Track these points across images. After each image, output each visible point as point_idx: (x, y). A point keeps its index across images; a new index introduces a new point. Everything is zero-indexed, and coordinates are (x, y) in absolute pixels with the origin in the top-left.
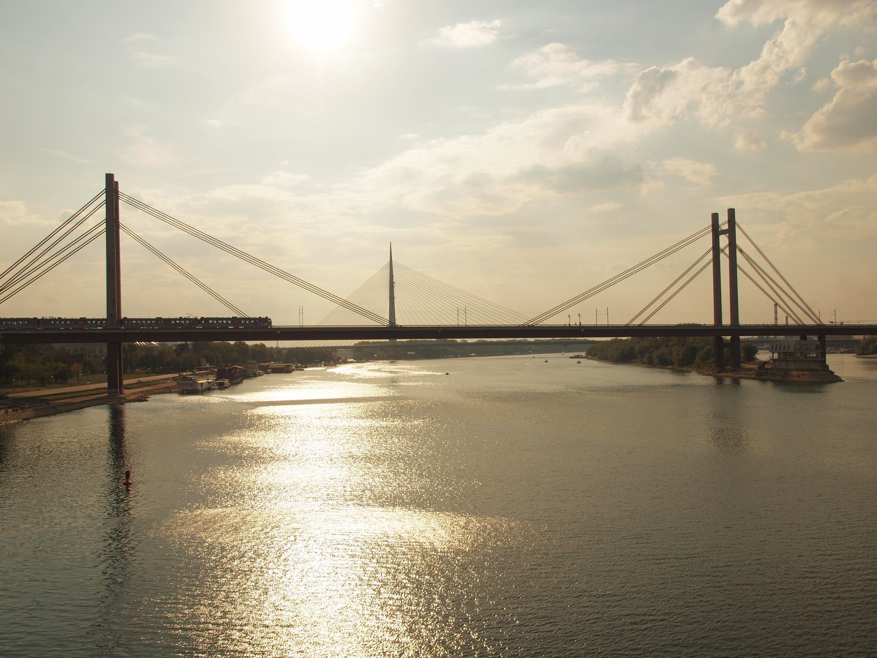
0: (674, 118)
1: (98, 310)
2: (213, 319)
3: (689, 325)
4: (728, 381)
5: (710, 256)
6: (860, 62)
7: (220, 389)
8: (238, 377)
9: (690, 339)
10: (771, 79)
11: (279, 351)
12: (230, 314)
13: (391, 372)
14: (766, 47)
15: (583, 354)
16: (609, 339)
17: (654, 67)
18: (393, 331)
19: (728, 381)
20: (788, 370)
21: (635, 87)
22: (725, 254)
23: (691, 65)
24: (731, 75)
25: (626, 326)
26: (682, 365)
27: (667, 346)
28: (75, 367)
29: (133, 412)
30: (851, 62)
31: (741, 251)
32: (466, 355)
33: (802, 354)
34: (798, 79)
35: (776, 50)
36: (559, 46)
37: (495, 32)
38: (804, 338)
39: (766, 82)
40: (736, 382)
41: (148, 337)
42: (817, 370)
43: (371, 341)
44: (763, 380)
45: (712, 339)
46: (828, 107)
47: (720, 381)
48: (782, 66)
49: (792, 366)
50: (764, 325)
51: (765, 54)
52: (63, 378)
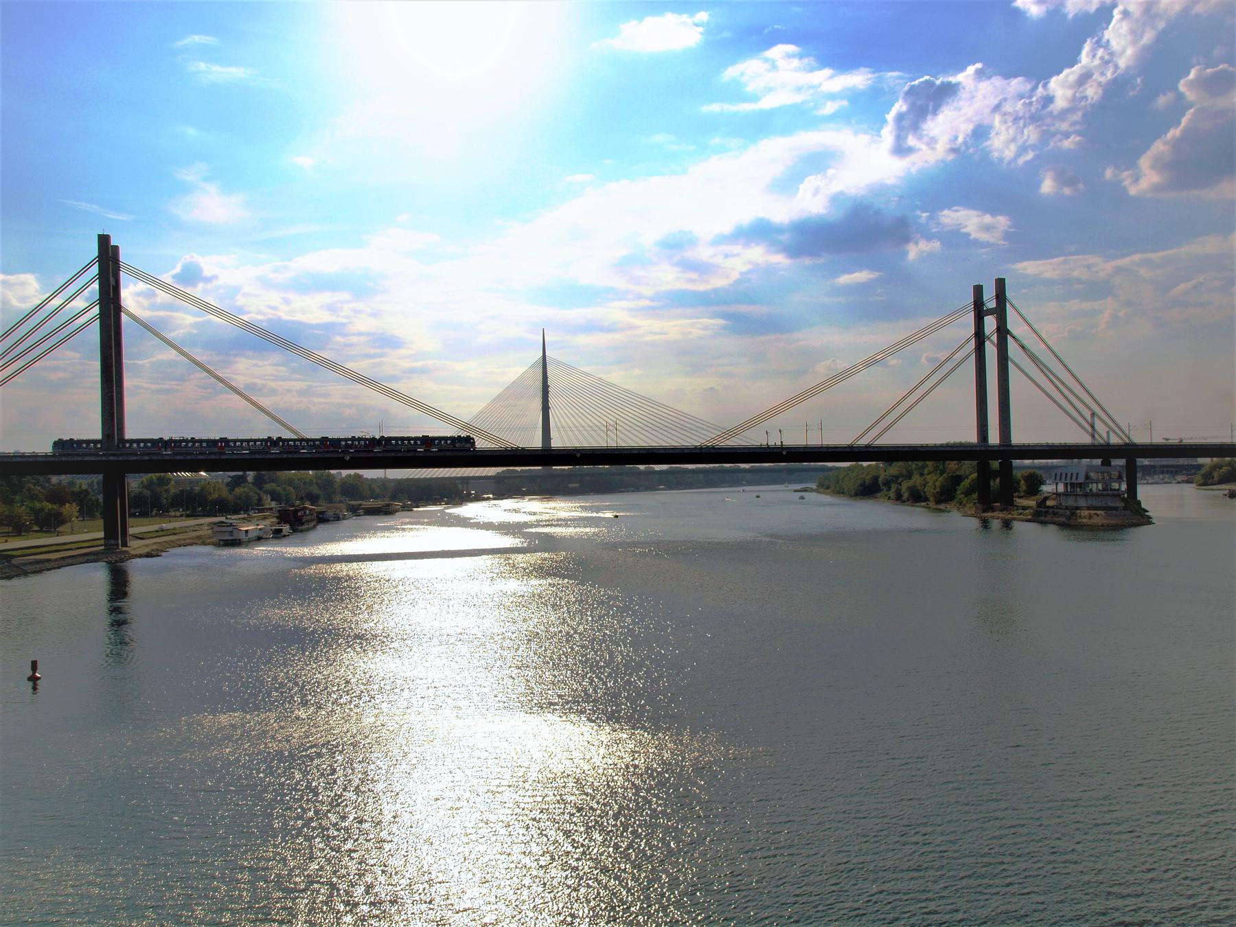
0: (953, 150)
1: (90, 428)
2: (396, 439)
3: (961, 445)
4: (996, 524)
6: (1221, 67)
8: (308, 521)
9: (952, 465)
11: (384, 483)
13: (530, 513)
14: (1087, 48)
17: (927, 77)
18: (547, 456)
19: (996, 524)
20: (1077, 508)
21: (900, 106)
22: (992, 342)
23: (980, 74)
24: (1035, 88)
26: (938, 502)
27: (922, 475)
29: (138, 570)
32: (651, 488)
33: (1104, 485)
35: (1100, 52)
36: (791, 48)
37: (701, 29)
38: (1106, 463)
39: (1086, 98)
40: (1007, 525)
41: (194, 466)
42: (1116, 509)
43: (518, 469)
44: (1044, 523)
46: (1174, 133)
47: (985, 524)
48: (1109, 75)
49: (1082, 502)
50: (1048, 445)
52: (50, 523)
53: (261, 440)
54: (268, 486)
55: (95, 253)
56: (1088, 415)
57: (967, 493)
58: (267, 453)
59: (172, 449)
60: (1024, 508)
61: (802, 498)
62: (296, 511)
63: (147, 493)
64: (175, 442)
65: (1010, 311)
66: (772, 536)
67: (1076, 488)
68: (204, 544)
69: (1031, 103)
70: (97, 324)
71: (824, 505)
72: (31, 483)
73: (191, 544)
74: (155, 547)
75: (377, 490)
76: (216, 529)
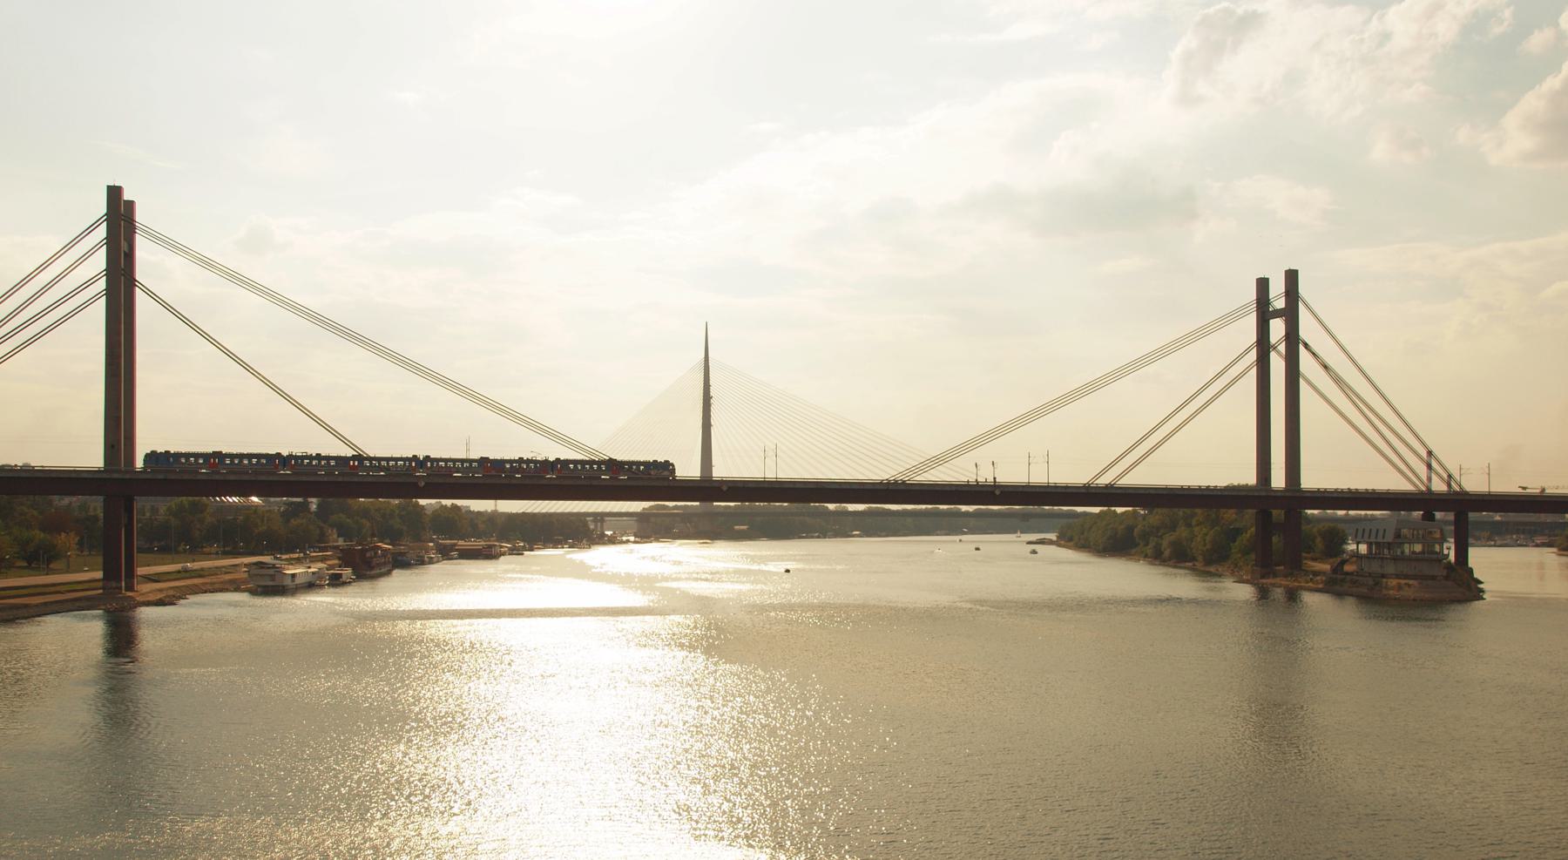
4: (1278, 593)
5: (1253, 356)
7: (331, 585)
8: (379, 565)
11: (493, 517)
12: (348, 452)
16: (1096, 510)
17: (1225, 4)
18: (707, 489)
20: (1383, 576)
22: (1279, 353)
24: (1367, 21)
25: (1087, 487)
26: (1208, 562)
27: (1189, 525)
28: (62, 539)
31: (1306, 345)
32: (843, 533)
34: (1497, 30)
40: (1292, 596)
41: (243, 489)
42: (1433, 578)
44: (1339, 595)
45: (1250, 513)
47: (1263, 594)
49: (1390, 569)
52: (40, 557)
53: (407, 459)
55: (101, 208)
58: (411, 475)
59: (292, 467)
60: (1316, 573)
61: (1034, 552)
62: (363, 551)
64: (296, 458)
66: (971, 601)
68: (237, 590)
69: (1362, 41)
70: (102, 303)
71: (1060, 562)
73: (221, 590)
74: (171, 593)
75: (482, 526)
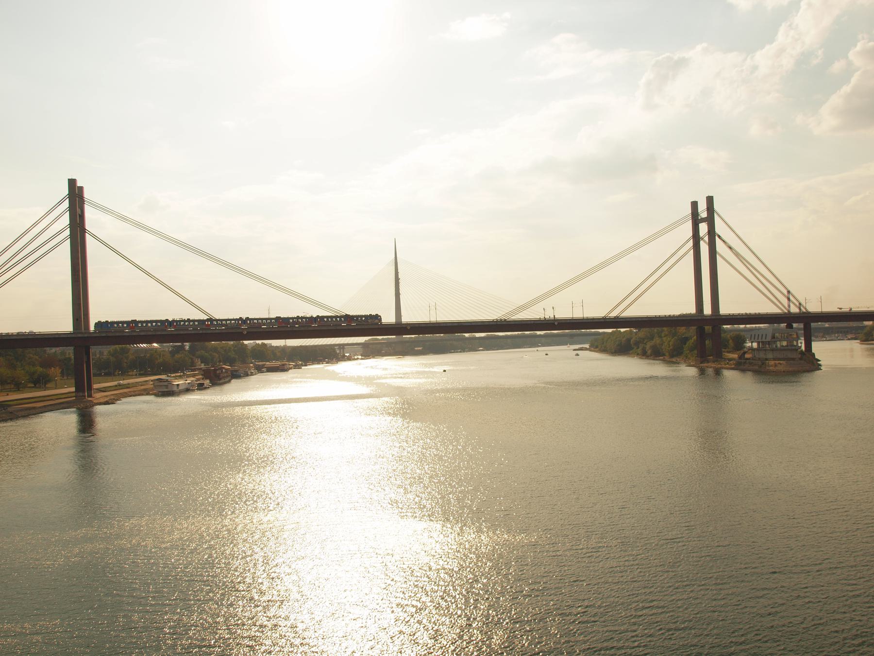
4: (710, 371)
5: (691, 243)
8: (224, 377)
9: (682, 330)
10: (787, 62)
11: (284, 349)
14: (782, 29)
15: (587, 346)
16: (610, 331)
17: (668, 54)
18: (399, 328)
20: (766, 359)
22: (705, 241)
24: (745, 59)
25: (604, 318)
26: (672, 356)
27: (660, 337)
29: (106, 416)
30: (870, 41)
31: (719, 237)
32: (474, 349)
33: (782, 345)
38: (790, 326)
40: (718, 372)
41: (149, 339)
42: (793, 359)
44: (743, 371)
46: (846, 89)
47: (702, 372)
51: (780, 37)
52: (40, 381)
54: (198, 353)
56: (785, 292)
57: (691, 350)
59: (175, 327)
60: (730, 360)
61: (577, 355)
63: (112, 359)
64: (177, 321)
65: (717, 219)
66: (547, 383)
67: (764, 345)
68: (148, 394)
70: (692, 251)
71: (591, 360)
72: (31, 354)
75: (278, 354)
76: (157, 383)
